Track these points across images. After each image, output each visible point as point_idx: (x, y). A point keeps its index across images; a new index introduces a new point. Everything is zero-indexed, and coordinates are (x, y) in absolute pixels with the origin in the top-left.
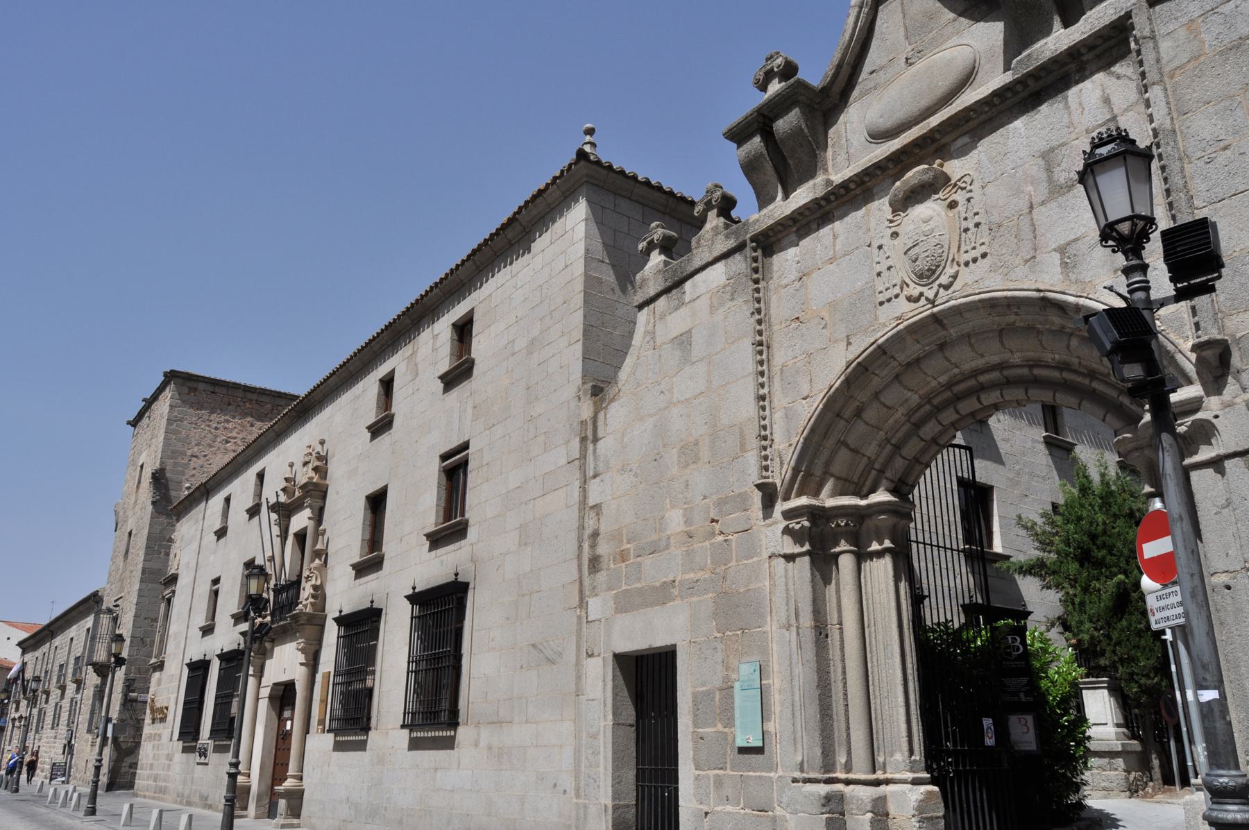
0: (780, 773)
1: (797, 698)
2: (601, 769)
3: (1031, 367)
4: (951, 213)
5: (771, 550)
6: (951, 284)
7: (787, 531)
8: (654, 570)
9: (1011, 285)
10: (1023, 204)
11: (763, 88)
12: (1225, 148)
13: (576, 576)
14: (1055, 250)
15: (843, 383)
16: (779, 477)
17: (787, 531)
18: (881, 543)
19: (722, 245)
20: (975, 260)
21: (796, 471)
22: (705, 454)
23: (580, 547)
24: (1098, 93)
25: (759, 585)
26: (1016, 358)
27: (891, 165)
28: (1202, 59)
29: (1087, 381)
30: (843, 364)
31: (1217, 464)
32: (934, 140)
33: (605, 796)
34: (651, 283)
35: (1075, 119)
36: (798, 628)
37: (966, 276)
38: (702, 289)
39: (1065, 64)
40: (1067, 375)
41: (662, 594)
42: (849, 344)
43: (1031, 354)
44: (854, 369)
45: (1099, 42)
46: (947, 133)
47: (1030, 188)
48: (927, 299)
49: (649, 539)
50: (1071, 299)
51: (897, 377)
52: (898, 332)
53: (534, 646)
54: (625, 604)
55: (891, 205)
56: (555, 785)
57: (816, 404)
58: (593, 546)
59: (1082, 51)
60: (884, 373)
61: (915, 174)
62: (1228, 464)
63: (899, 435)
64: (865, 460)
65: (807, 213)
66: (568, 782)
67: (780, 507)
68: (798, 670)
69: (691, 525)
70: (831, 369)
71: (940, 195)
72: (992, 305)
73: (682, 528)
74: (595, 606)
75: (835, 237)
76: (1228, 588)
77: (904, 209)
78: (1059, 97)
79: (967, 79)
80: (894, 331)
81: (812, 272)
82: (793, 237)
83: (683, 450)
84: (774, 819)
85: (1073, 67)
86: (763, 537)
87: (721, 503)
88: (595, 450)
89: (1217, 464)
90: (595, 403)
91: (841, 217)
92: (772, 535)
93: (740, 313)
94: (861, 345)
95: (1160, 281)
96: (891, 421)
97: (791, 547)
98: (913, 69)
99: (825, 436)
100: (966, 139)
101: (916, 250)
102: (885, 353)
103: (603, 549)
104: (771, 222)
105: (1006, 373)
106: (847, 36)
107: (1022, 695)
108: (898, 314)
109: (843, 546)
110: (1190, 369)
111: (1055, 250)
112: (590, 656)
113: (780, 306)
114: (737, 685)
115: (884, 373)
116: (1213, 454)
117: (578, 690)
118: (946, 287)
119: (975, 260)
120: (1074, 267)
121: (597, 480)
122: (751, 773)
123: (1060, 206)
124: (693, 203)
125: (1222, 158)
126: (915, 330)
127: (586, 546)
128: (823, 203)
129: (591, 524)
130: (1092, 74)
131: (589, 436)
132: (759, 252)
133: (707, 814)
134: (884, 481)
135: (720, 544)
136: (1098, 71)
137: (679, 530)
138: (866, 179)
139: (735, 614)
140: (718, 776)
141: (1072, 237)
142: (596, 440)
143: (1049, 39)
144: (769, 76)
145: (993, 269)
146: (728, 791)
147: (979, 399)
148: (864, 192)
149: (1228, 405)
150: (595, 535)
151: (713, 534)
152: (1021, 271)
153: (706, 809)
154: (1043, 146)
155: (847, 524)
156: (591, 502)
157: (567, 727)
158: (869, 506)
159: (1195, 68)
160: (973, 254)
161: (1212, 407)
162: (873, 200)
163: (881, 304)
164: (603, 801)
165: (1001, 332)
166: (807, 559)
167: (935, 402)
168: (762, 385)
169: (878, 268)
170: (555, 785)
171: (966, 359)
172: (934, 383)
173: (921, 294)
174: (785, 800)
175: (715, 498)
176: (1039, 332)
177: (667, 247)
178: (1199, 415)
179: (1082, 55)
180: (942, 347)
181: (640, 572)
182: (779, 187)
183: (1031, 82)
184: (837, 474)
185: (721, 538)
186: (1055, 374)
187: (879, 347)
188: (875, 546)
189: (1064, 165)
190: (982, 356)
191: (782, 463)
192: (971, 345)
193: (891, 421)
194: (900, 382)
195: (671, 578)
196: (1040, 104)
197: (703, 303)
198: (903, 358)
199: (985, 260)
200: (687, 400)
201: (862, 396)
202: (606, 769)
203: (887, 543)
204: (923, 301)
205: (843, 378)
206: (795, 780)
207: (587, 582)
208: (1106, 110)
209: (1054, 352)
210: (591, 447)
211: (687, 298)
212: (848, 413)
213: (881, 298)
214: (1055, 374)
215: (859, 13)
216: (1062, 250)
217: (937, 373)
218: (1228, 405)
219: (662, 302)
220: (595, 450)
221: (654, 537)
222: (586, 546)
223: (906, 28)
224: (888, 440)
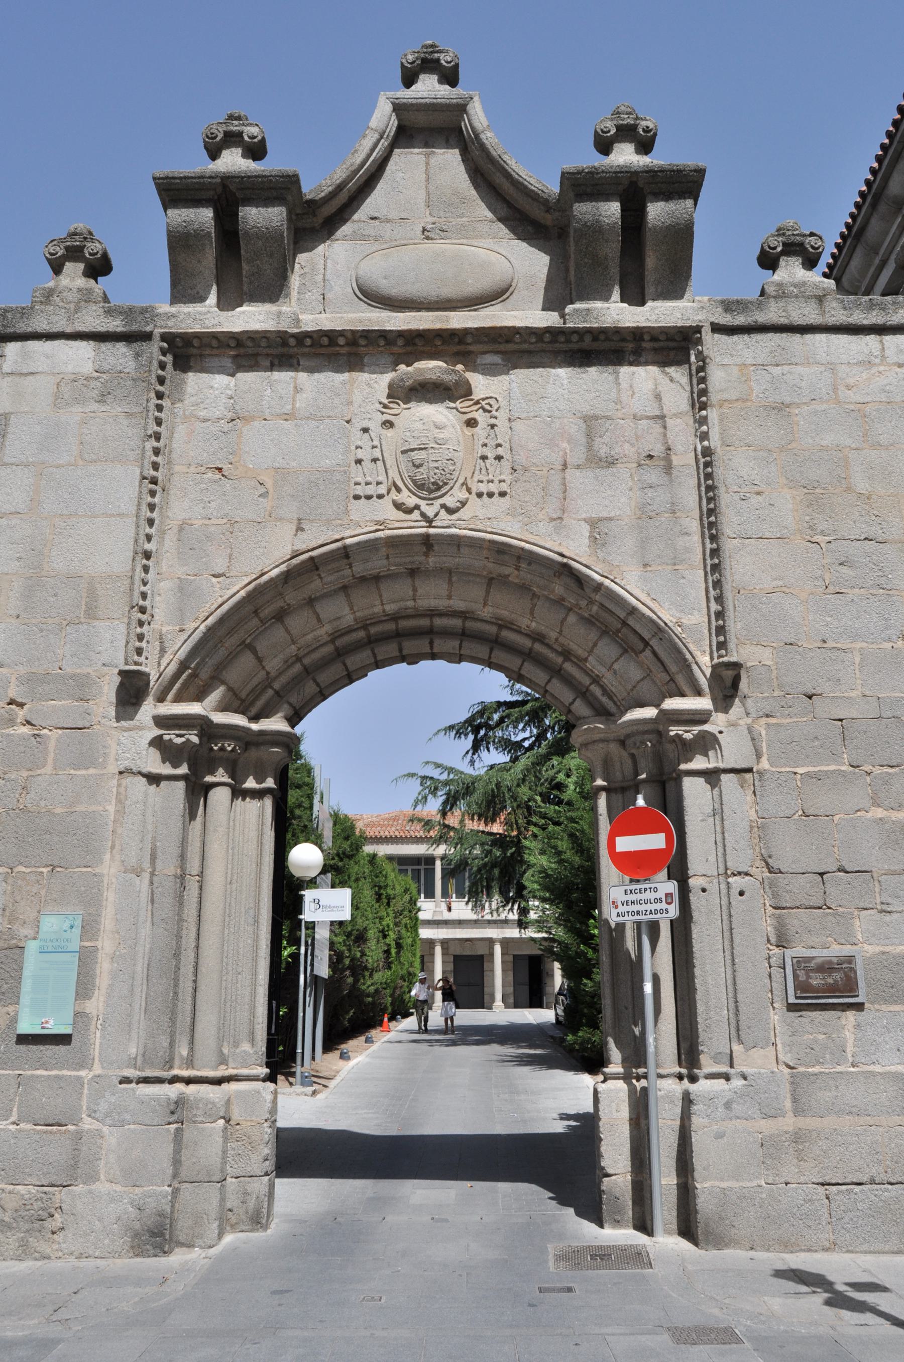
0: (97, 1070)
1: (139, 969)
3: (501, 627)
4: (468, 431)
6: (456, 510)
7: (157, 742)
9: (531, 538)
11: (214, 153)
12: (758, 493)
14: (585, 520)
15: (282, 573)
16: (157, 667)
17: (157, 742)
18: (260, 780)
20: (491, 495)
21: (183, 666)
24: (650, 385)
25: (94, 808)
27: (400, 342)
28: (749, 404)
29: (560, 660)
30: (287, 552)
31: (712, 776)
32: (461, 342)
35: (624, 398)
36: (152, 874)
37: (475, 509)
38: (40, 365)
39: (623, 340)
42: (300, 529)
43: (505, 613)
44: (303, 562)
45: (662, 337)
47: (565, 445)
48: (423, 515)
51: (345, 588)
52: (376, 539)
55: (390, 386)
57: (236, 588)
59: (646, 337)
60: (330, 579)
61: (431, 367)
62: (724, 777)
63: (316, 656)
65: (264, 343)
67: (149, 709)
68: (145, 931)
70: (270, 552)
71: (458, 404)
72: (501, 551)
75: (297, 390)
76: (704, 890)
77: (407, 401)
78: (610, 369)
79: (498, 294)
80: (372, 536)
81: (253, 419)
82: (228, 362)
84: (79, 1136)
85: (630, 346)
87: (30, 680)
89: (712, 776)
91: (311, 370)
92: (134, 742)
94: (317, 538)
97: (155, 764)
98: (428, 246)
99: (230, 633)
100: (497, 359)
101: (422, 455)
102: (347, 556)
104: (197, 329)
106: (359, 159)
108: (380, 518)
109: (221, 776)
110: (704, 683)
111: (585, 520)
113: (186, 442)
114: (32, 947)
116: (711, 766)
118: (451, 511)
119: (491, 495)
120: (604, 545)
122: (40, 1072)
123: (596, 478)
125: (755, 500)
126: (396, 543)
128: (292, 342)
130: (647, 363)
132: (169, 359)
134: (286, 706)
135: (22, 737)
136: (653, 363)
138: (363, 342)
141: (606, 515)
143: (598, 305)
144: (232, 139)
145: (511, 512)
147: (431, 643)
148: (350, 354)
149: (733, 725)
151: (12, 722)
152: (544, 527)
154: (586, 409)
155: (233, 750)
158: (262, 733)
159: (742, 409)
160: (493, 487)
161: (717, 723)
162: (362, 370)
163: (357, 497)
165: (490, 581)
166: (181, 785)
167: (373, 630)
168: (149, 538)
169: (360, 454)
171: (432, 595)
172: (378, 609)
173: (417, 507)
175: (22, 670)
176: (534, 595)
178: (706, 727)
179: (644, 340)
180: (413, 573)
182: (215, 287)
183: (588, 339)
185: (26, 730)
186: (527, 643)
187: (345, 547)
188: (250, 783)
189: (606, 439)
191: (163, 651)
192: (450, 582)
194: (348, 596)
196: (590, 365)
198: (359, 569)
199: (502, 500)
201: (292, 597)
203: (270, 783)
204: (416, 515)
205: (283, 568)
206: (126, 1080)
208: (656, 405)
209: (543, 620)
212: (266, 612)
213: (359, 490)
214: (527, 643)
215: (378, 141)
216: (593, 523)
217: (394, 598)
218: (733, 725)
223: (428, 194)
224: (299, 659)
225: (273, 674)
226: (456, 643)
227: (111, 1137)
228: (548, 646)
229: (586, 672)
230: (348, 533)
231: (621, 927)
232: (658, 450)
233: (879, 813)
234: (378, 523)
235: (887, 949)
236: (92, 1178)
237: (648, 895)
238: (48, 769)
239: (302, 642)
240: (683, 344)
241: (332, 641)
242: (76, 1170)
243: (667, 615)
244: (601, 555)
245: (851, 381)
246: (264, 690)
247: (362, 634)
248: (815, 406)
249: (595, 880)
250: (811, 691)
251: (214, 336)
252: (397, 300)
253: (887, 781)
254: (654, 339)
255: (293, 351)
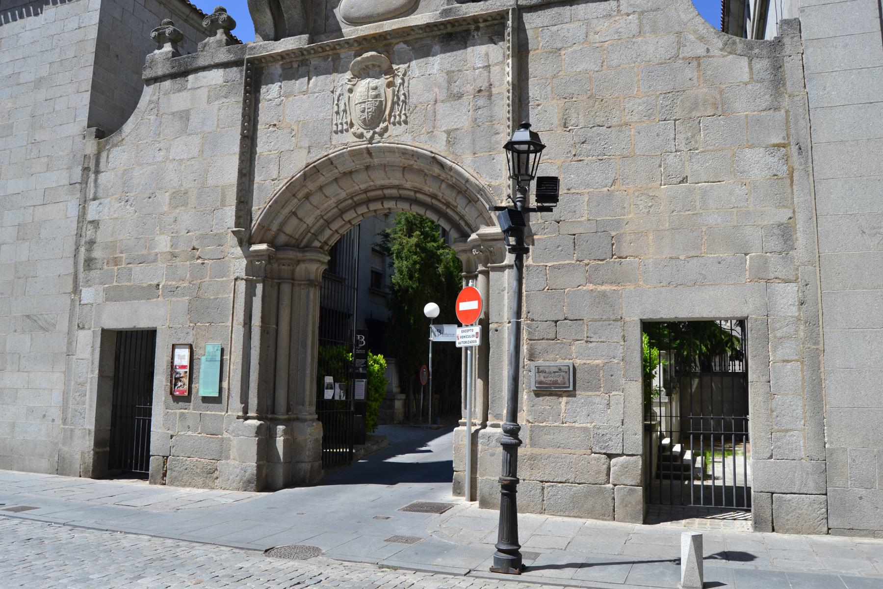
2: (87, 406)
3: (416, 192)
5: (236, 275)
8: (141, 275)
9: (417, 144)
10: (431, 97)
13: (72, 271)
19: (223, 55)
22: (193, 201)
23: (77, 249)
26: (408, 185)
29: (444, 208)
32: (385, 39)
33: (90, 424)
34: (159, 66)
38: (203, 82)
39: (469, 24)
40: (434, 201)
41: (152, 291)
43: (417, 185)
45: (490, 19)
46: (394, 38)
47: (436, 90)
49: (140, 253)
50: (449, 162)
51: (336, 179)
53: (28, 316)
54: (114, 295)
56: (44, 416)
58: (89, 250)
59: (481, 20)
63: (330, 214)
64: (305, 226)
66: (56, 414)
69: (176, 248)
70: (295, 165)
73: (168, 249)
74: (88, 295)
83: (173, 197)
84: (222, 440)
86: (231, 265)
87: (202, 237)
88: (96, 181)
90: (99, 144)
93: (232, 108)
94: (317, 155)
95: (533, 203)
96: (326, 205)
102: (332, 163)
103: (97, 253)
105: (401, 192)
107: (361, 369)
112: (81, 327)
115: (328, 175)
117: (68, 350)
121: (96, 202)
124: (202, 16)
126: (355, 154)
127: (83, 250)
129: (89, 233)
131: (92, 168)
133: (172, 437)
135: (198, 264)
137: (165, 250)
138: (337, 47)
139: (200, 309)
140: (183, 413)
141: (455, 127)
142: (97, 172)
146: (190, 422)
147: (382, 204)
150: (92, 243)
152: (424, 138)
153: (171, 432)
156: (90, 217)
157: (58, 377)
164: (88, 427)
167: (355, 199)
170: (44, 416)
171: (380, 179)
172: (357, 188)
174: (231, 428)
176: (426, 175)
177: (176, 39)
181: (130, 275)
183: (449, 26)
184: (287, 232)
187: (329, 159)
190: (389, 179)
192: (385, 171)
193: (326, 205)
194: (337, 183)
195: (156, 282)
197: (203, 93)
198: (342, 169)
200: (182, 160)
201: (312, 186)
202: (91, 406)
207: (81, 276)
209: (430, 187)
210: (92, 177)
211: (189, 86)
212: (300, 195)
214: (428, 199)
216: (448, 133)
217: (361, 183)
219: (167, 84)
220: (96, 181)
221: (145, 252)
222: (83, 250)
224: (322, 217)
225: (310, 225)
226: (394, 203)
227: (235, 441)
228: (439, 201)
229: (457, 214)
230: (331, 151)
231: (461, 348)
232: (485, 85)
233: (591, 287)
234: (344, 144)
235: (588, 362)
236: (228, 458)
237: (470, 333)
238: (207, 279)
239: (322, 208)
240: (502, 21)
241: (337, 207)
242: (222, 453)
243: (483, 181)
244: (451, 150)
245: (598, 29)
246: (306, 234)
247: (350, 201)
248: (575, 47)
249: (684, 322)
250: (558, 219)
251: (271, 56)
252: (358, 18)
253: (596, 269)
254: (485, 21)
255: (307, 57)
